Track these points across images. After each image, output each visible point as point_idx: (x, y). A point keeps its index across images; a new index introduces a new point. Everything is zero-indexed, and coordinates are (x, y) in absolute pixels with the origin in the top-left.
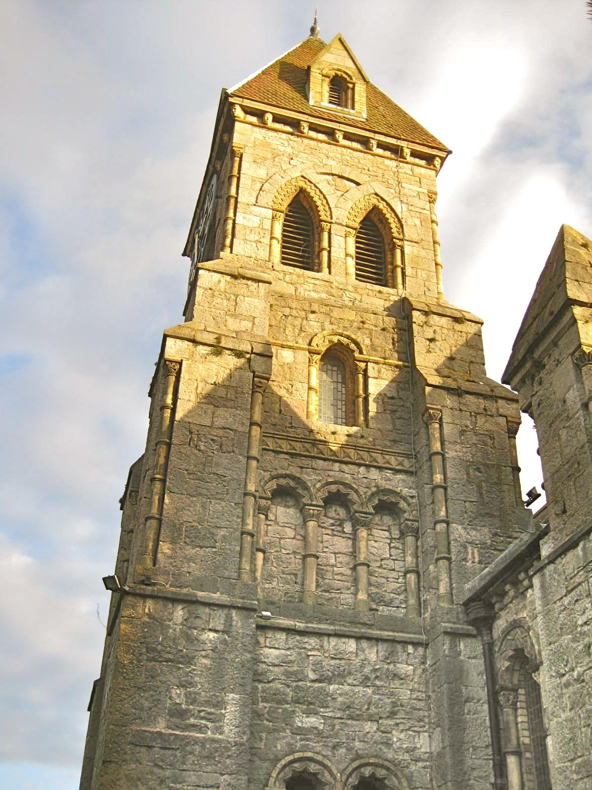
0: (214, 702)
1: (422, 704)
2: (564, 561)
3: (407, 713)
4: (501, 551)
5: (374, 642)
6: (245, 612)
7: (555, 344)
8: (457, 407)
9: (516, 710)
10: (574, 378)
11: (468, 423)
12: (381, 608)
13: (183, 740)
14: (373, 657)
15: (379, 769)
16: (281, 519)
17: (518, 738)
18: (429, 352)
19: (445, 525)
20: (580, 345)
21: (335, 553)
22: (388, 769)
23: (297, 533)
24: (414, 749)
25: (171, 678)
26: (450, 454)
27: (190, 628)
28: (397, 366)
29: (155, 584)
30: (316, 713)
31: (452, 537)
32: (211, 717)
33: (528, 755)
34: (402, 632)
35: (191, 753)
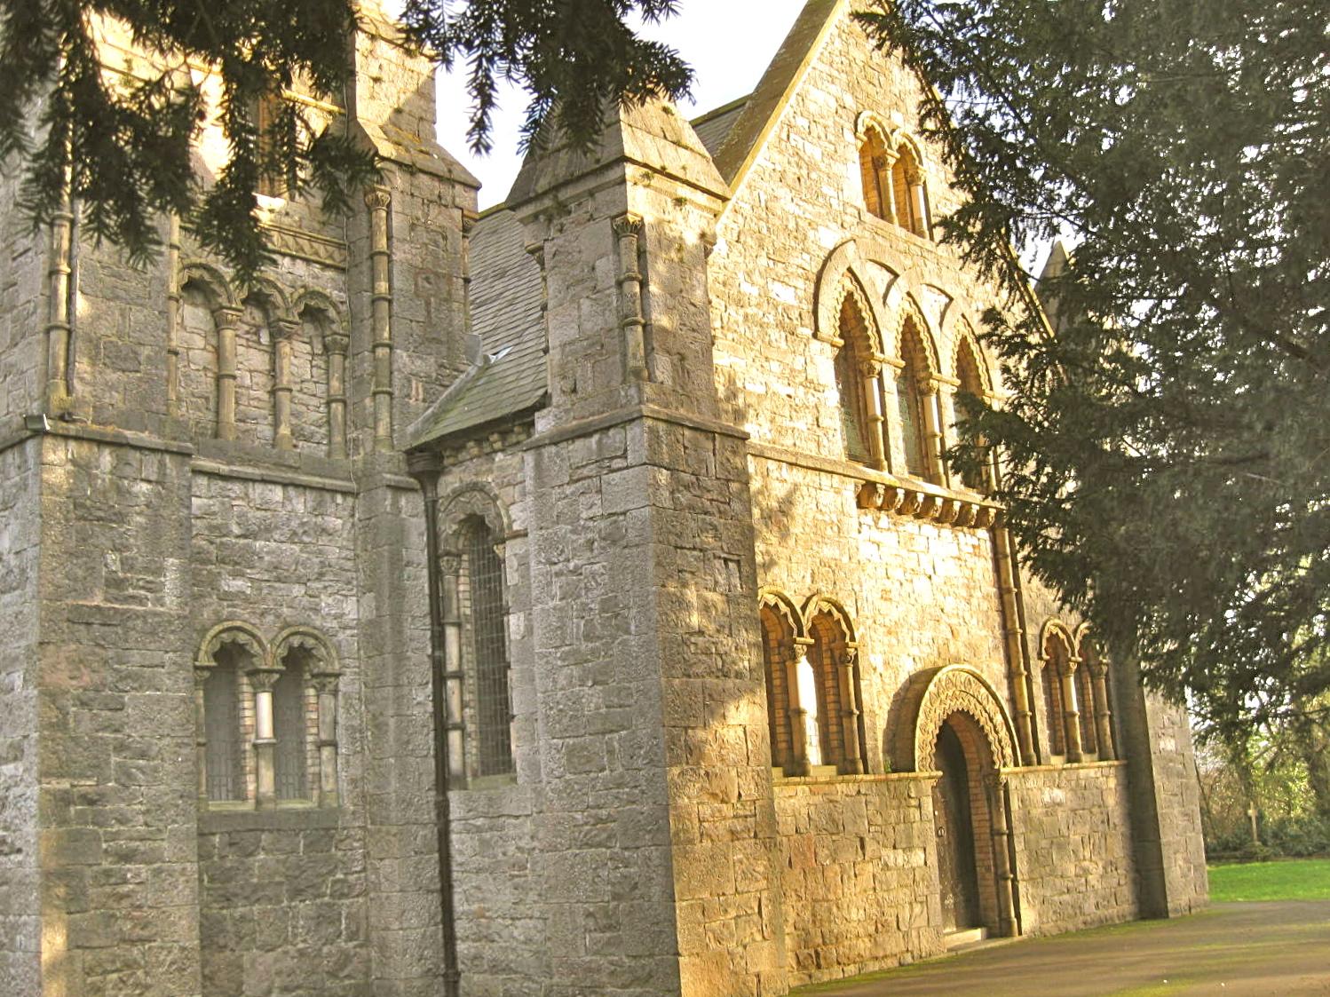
0: (153, 567)
1: (349, 564)
2: (571, 447)
3: (335, 575)
4: (447, 387)
5: (301, 490)
6: (180, 458)
7: (591, 194)
8: (408, 190)
9: (458, 577)
10: (610, 246)
11: (420, 214)
12: (301, 443)
13: (123, 614)
14: (300, 508)
15: (307, 638)
16: (189, 322)
17: (458, 608)
18: (372, 97)
19: (388, 350)
20: (625, 212)
21: (250, 371)
22: (316, 638)
23: (207, 343)
24: (342, 615)
25: (102, 540)
26: (398, 256)
27: (121, 478)
28: (330, 113)
29: (74, 421)
30: (243, 575)
31: (395, 366)
32: (150, 586)
33: (469, 627)
34: (331, 477)
35: (134, 629)
